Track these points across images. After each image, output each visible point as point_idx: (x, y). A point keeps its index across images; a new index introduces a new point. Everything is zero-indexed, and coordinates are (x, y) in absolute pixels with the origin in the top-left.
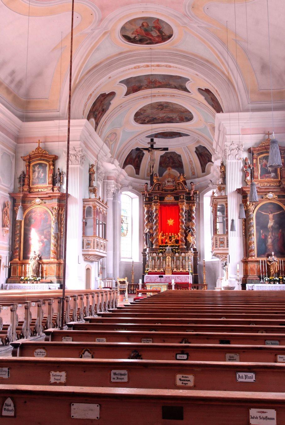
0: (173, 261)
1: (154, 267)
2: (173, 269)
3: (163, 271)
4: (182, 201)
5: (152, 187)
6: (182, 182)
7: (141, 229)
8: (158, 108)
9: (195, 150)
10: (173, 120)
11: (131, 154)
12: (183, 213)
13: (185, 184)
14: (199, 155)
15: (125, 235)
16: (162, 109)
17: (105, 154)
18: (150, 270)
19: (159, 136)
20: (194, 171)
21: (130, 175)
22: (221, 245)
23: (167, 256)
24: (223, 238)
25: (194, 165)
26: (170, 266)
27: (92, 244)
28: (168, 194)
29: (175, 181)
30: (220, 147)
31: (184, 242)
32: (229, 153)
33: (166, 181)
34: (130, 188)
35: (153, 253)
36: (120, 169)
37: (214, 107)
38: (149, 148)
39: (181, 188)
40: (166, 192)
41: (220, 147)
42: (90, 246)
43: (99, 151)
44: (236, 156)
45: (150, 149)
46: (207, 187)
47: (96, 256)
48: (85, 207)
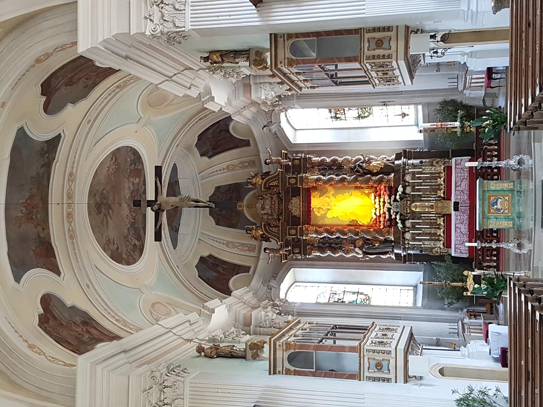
0: (422, 199)
1: (434, 237)
2: (439, 197)
3: (442, 219)
4: (300, 180)
5: (271, 239)
6: (263, 179)
7: (355, 264)
8: (105, 215)
9: (205, 159)
10: (138, 190)
11: (208, 279)
12: (325, 178)
13: (268, 173)
14: (216, 151)
15: (369, 299)
16: (110, 207)
17: (188, 324)
18: (440, 244)
19: (174, 224)
20: (246, 162)
21: (248, 284)
22: (386, 45)
23: (410, 209)
24: (368, 41)
25: (235, 162)
26: (432, 204)
27: (380, 357)
28: (287, 208)
29: (262, 196)
30: (175, 74)
31: (382, 178)
32: (171, 25)
33: (262, 212)
34: (273, 283)
35: (404, 238)
36: (229, 300)
37: (90, 82)
38: (152, 210)
39: (274, 183)
40: (282, 213)
41: (175, 74)
42: (385, 363)
43: (175, 337)
44: (177, 10)
45: (156, 207)
46: (277, 137)
47: (410, 350)
48: (289, 370)
